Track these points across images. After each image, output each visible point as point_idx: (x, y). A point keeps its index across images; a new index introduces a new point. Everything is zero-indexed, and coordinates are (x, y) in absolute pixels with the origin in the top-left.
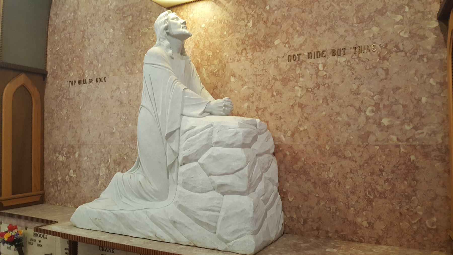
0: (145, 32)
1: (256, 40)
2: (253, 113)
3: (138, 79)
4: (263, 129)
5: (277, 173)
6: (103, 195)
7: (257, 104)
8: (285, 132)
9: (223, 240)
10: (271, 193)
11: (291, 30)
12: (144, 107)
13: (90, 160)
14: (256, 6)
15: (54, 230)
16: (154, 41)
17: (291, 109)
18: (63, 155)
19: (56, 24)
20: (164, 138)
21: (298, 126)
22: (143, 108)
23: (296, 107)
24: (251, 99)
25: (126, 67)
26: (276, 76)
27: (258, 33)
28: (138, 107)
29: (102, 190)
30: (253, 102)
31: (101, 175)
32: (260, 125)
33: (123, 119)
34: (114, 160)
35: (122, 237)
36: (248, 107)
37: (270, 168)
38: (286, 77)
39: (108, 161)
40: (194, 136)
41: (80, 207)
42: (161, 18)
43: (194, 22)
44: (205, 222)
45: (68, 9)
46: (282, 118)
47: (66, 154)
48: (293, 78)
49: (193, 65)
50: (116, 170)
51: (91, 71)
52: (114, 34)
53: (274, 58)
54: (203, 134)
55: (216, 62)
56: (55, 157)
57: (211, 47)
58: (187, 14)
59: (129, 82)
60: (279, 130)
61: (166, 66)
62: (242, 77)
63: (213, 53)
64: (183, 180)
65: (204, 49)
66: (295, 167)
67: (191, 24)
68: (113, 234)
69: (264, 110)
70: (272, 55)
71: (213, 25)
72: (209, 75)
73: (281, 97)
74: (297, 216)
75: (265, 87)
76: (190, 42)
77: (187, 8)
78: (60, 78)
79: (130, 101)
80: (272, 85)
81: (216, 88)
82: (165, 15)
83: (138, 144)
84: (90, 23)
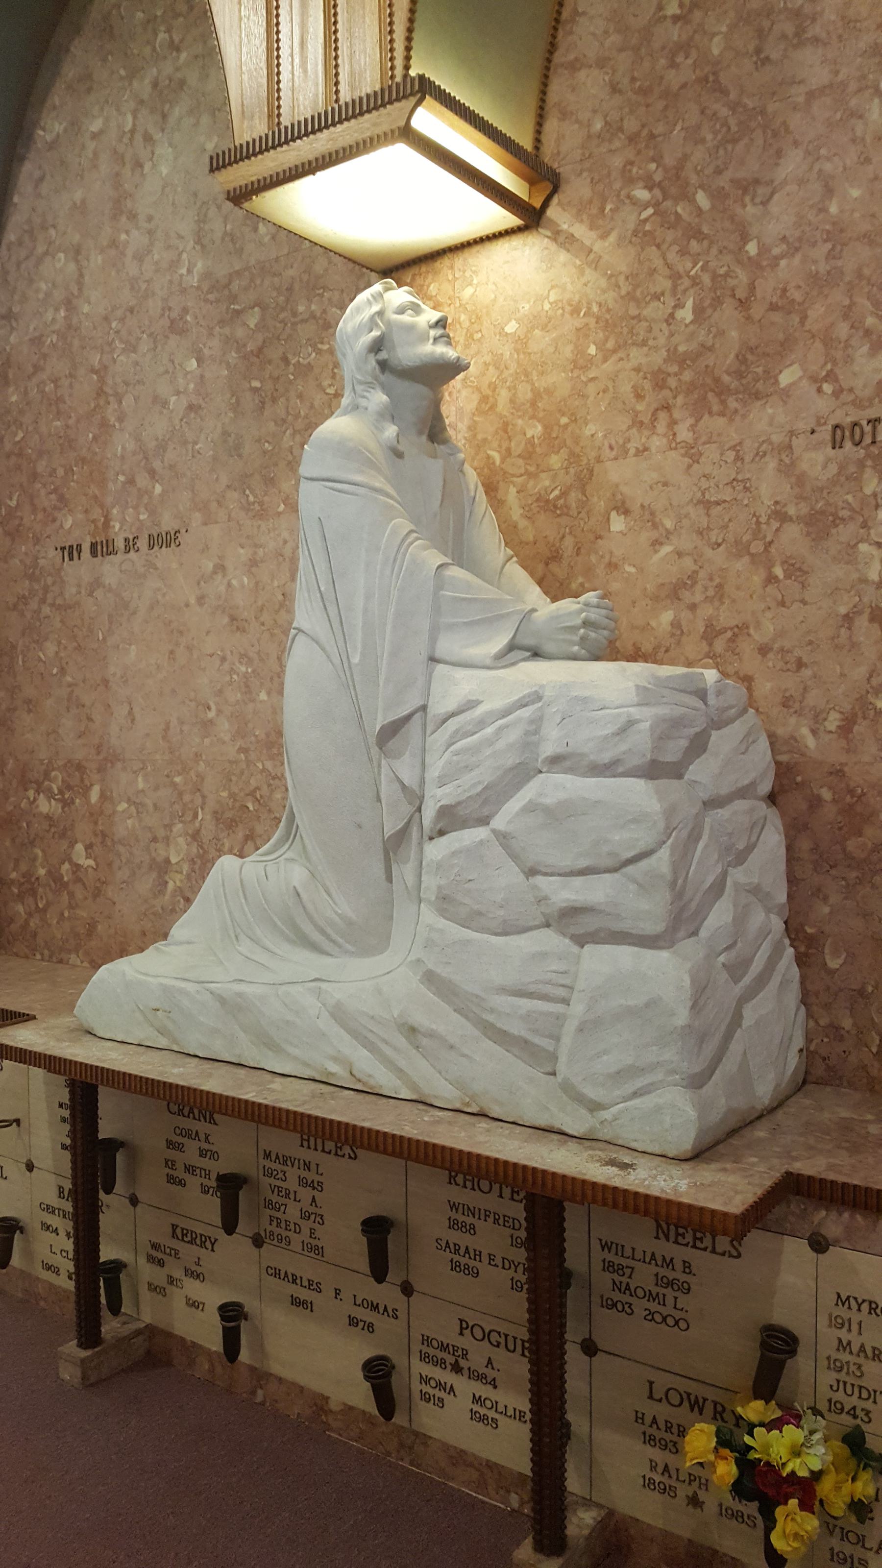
0: (305, 362)
1: (709, 370)
2: (692, 647)
3: (285, 535)
4: (731, 707)
5: (782, 867)
6: (177, 931)
7: (711, 611)
8: (818, 718)
9: (580, 1099)
10: (759, 943)
11: (843, 330)
12: (303, 632)
13: (138, 812)
14: (706, 243)
15: (20, 1045)
16: (338, 395)
17: (843, 630)
18: (50, 796)
19: (11, 349)
20: (372, 740)
21: (868, 692)
22: (301, 638)
23: (862, 622)
24: (686, 595)
25: (245, 491)
26: (785, 505)
27: (717, 346)
28: (286, 633)
29: (178, 909)
30: (693, 607)
31: (174, 860)
32: (719, 693)
33: (238, 675)
34: (216, 812)
35: (242, 1072)
36: (676, 624)
37: (755, 850)
38: (824, 508)
39: (196, 816)
40: (476, 737)
41: (104, 971)
42: (358, 310)
43: (477, 319)
44: (516, 1033)
45: (48, 295)
46: (806, 665)
47: (61, 792)
48: (852, 510)
49: (472, 476)
50: (223, 844)
51: (131, 510)
52: (202, 377)
53: (776, 438)
54: (507, 726)
55: (555, 461)
56: (25, 800)
57: (540, 405)
58: (454, 291)
59: (256, 546)
60: (792, 710)
61: (377, 485)
62: (652, 514)
63: (545, 427)
64: (440, 888)
65: (512, 413)
66: (851, 845)
67: (466, 324)
68: (211, 1062)
69: (735, 635)
70: (771, 424)
71: (546, 325)
72: (530, 510)
73: (802, 583)
74: (855, 1024)
75: (741, 549)
76: (464, 393)
77: (452, 268)
78: (31, 535)
79: (262, 609)
80: (768, 539)
81: (556, 557)
82: (371, 298)
83: (288, 758)
84: (121, 341)
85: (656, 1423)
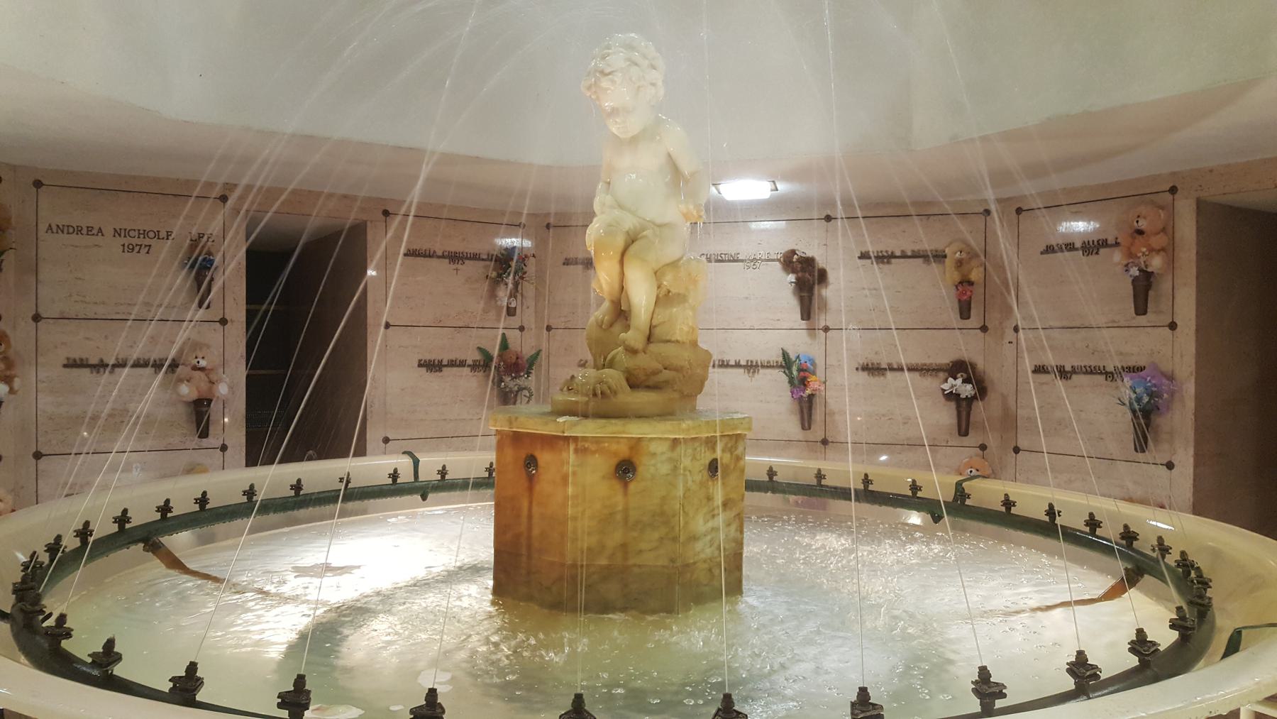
85: (101, 232)
